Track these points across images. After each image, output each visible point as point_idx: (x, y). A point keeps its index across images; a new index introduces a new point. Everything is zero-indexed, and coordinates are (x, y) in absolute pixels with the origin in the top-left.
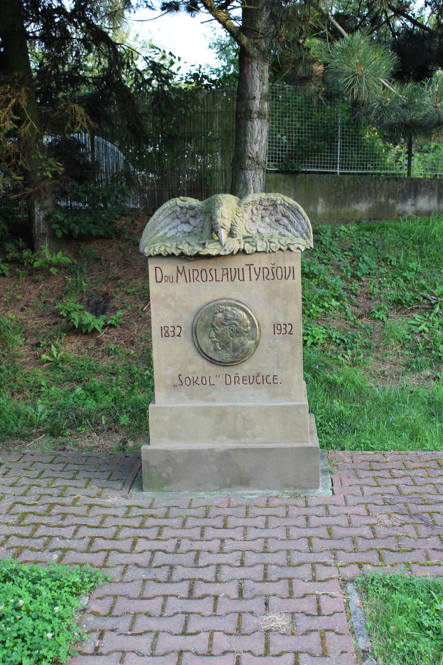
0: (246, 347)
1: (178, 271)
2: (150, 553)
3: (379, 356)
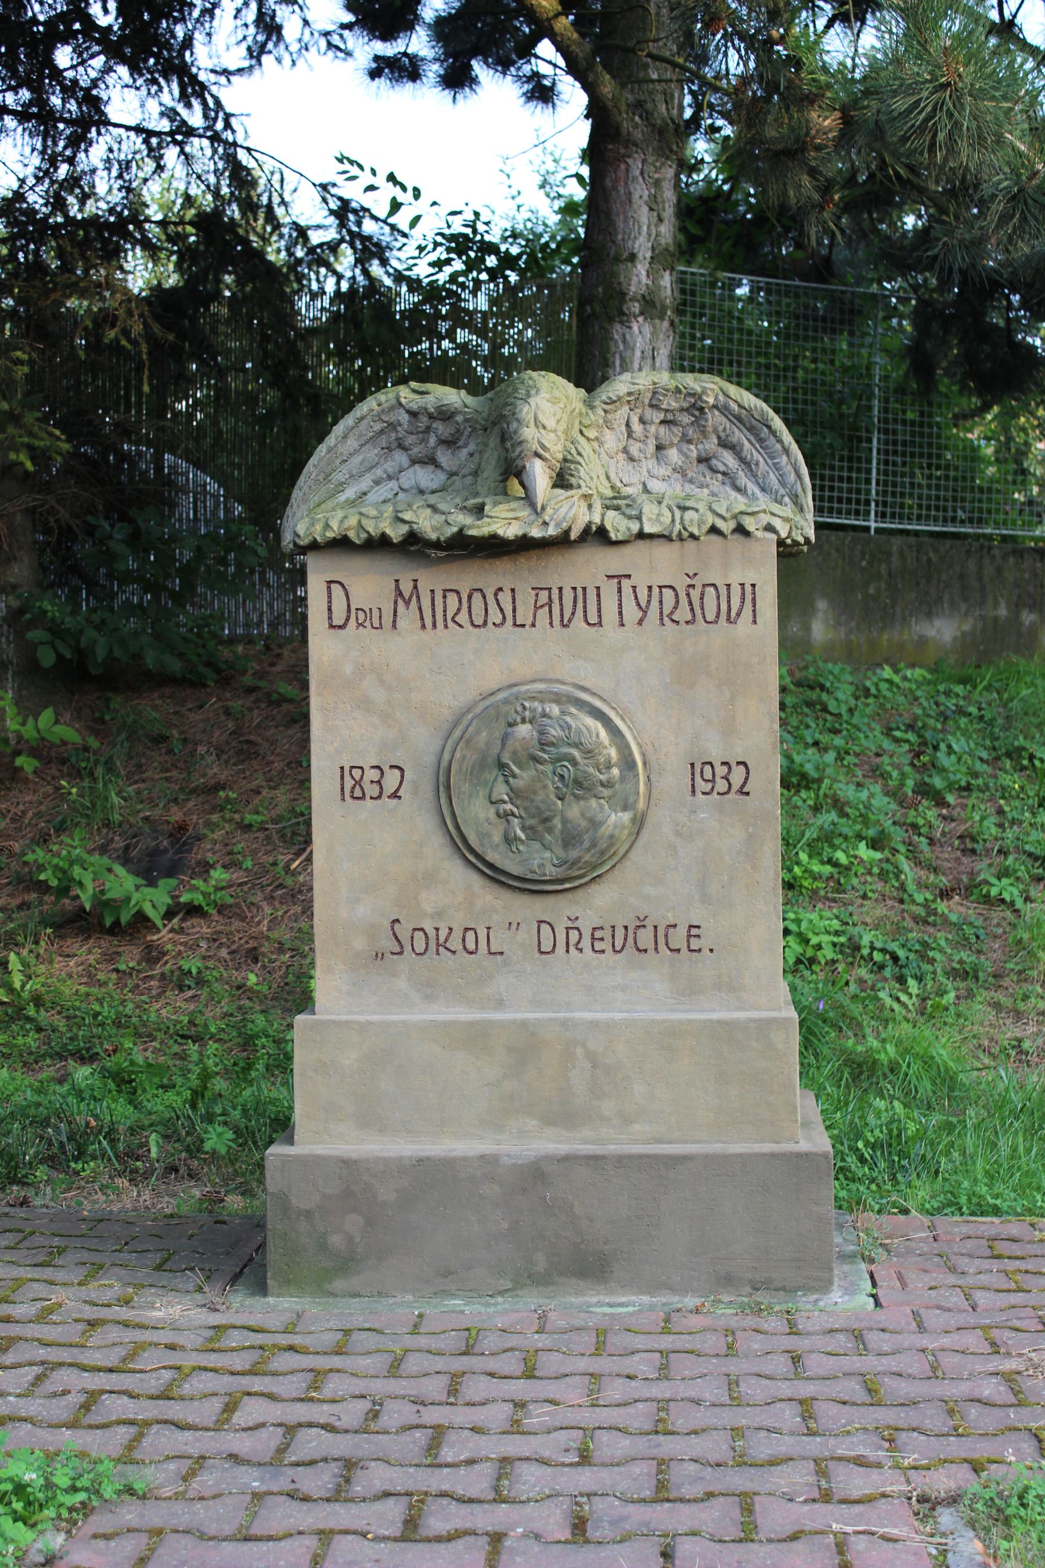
0: (605, 830)
2: (280, 1430)
3: (1003, 1000)
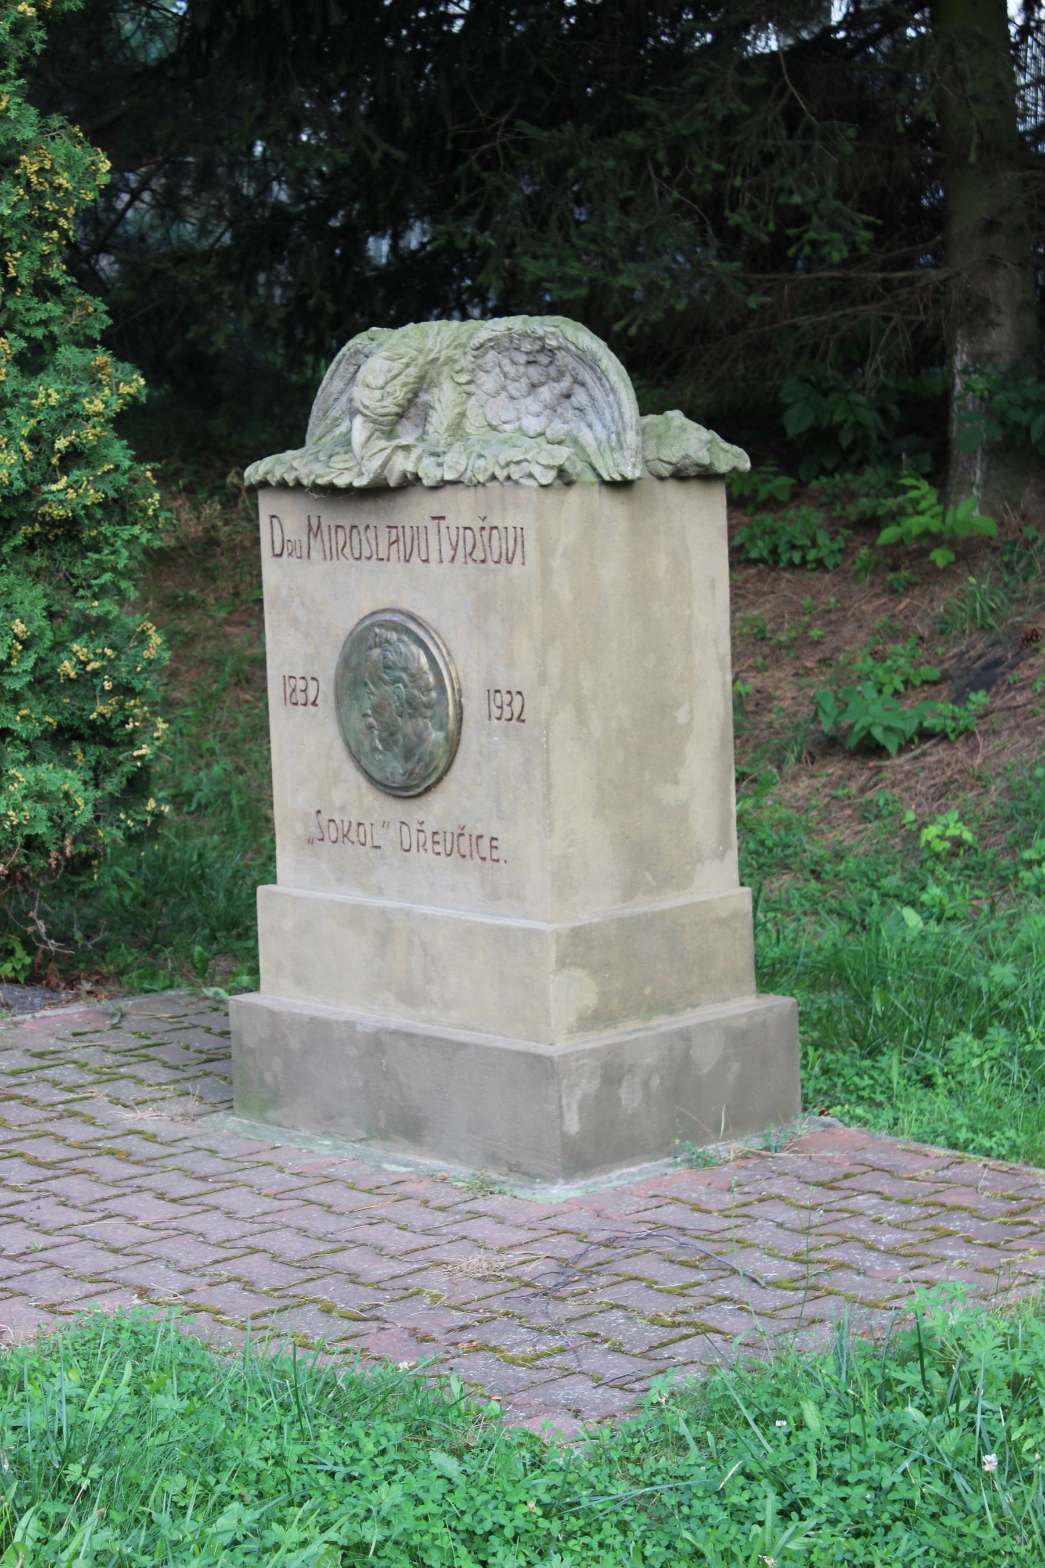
0: (426, 748)
1: (310, 529)
